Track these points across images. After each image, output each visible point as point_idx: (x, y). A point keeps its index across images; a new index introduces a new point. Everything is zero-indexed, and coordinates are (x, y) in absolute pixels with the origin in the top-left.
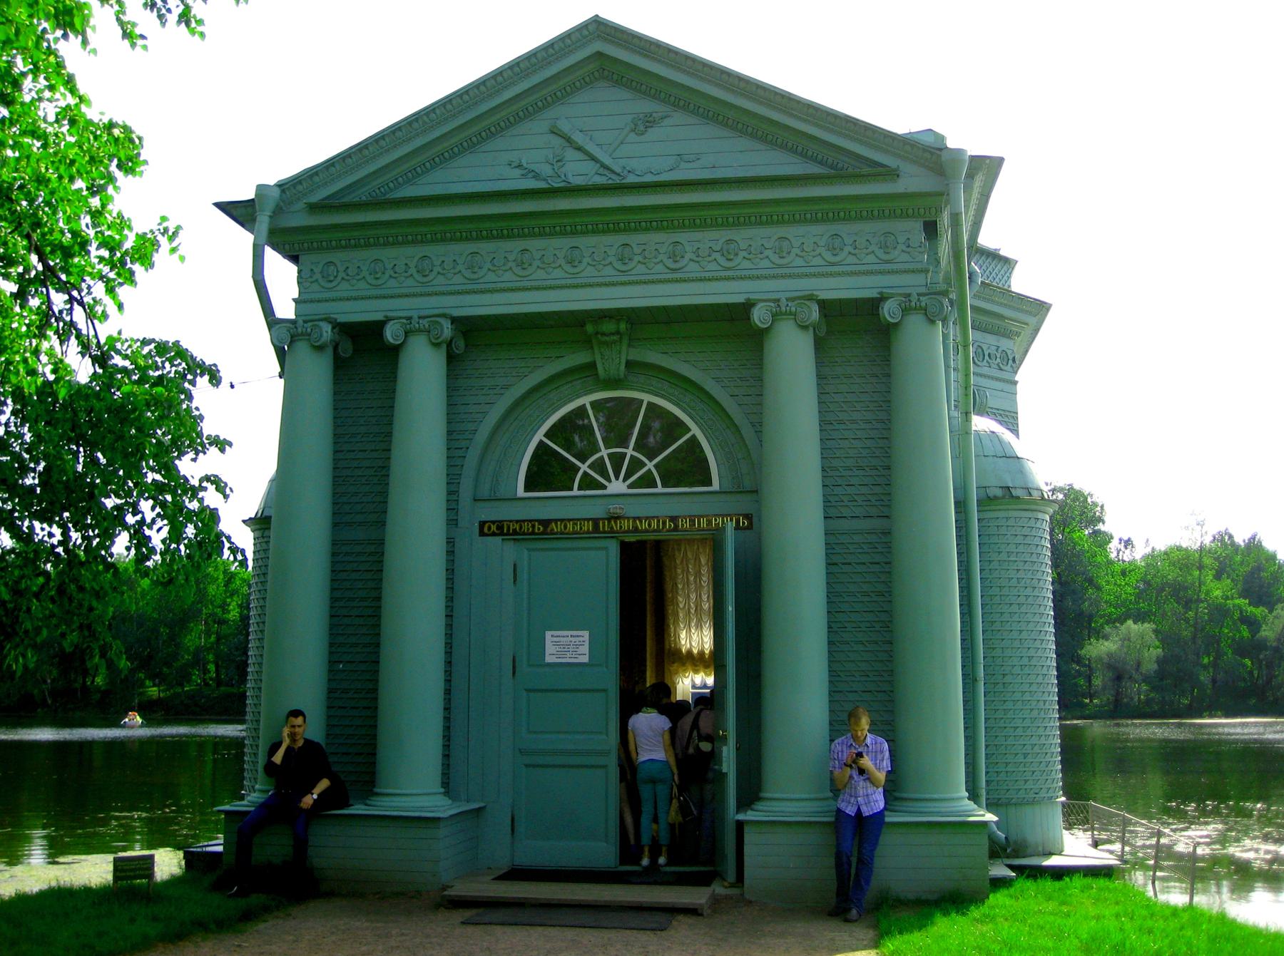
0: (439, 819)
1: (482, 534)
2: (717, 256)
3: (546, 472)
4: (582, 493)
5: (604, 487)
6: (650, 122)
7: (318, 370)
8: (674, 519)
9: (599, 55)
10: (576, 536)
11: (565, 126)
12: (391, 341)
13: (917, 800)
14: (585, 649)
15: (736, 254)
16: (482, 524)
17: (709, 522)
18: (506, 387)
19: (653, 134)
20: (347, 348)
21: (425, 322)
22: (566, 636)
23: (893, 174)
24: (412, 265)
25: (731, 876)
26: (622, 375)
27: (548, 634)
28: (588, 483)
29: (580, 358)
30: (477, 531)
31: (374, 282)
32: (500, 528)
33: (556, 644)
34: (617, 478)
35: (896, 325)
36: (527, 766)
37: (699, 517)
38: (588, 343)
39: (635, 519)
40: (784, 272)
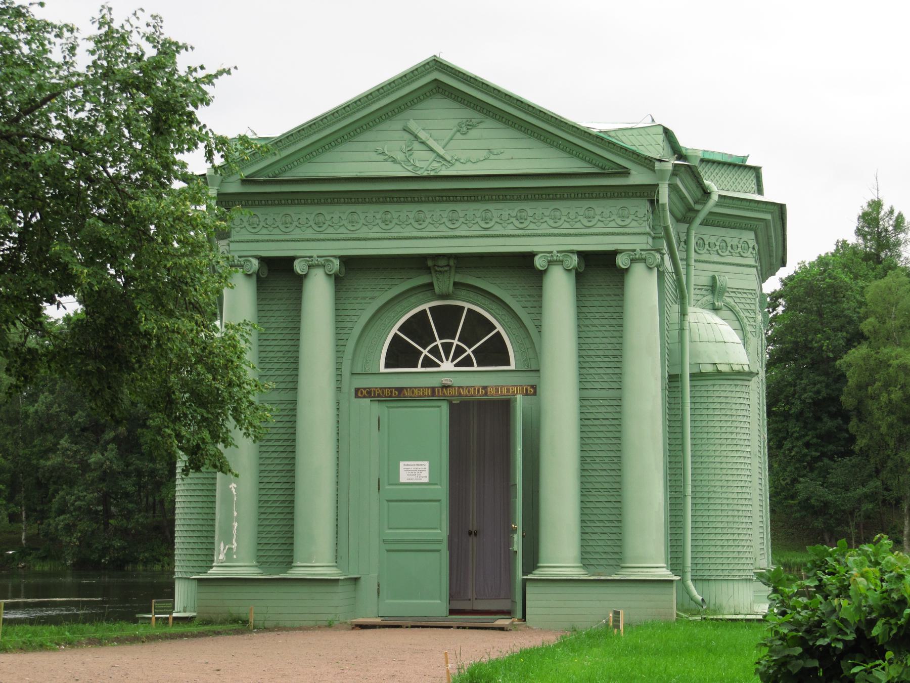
0: (338, 580)
1: (357, 396)
2: (513, 220)
3: (400, 355)
4: (424, 369)
5: (439, 366)
6: (470, 127)
8: (485, 388)
9: (436, 80)
12: (300, 272)
13: (623, 567)
14: (426, 473)
16: (357, 390)
17: (508, 390)
19: (473, 133)
22: (413, 465)
23: (626, 173)
25: (519, 614)
27: (402, 464)
28: (428, 363)
29: (423, 280)
31: (285, 230)
33: (407, 470)
34: (447, 360)
35: (627, 270)
36: (388, 551)
37: (502, 387)
38: (428, 270)
39: (459, 387)
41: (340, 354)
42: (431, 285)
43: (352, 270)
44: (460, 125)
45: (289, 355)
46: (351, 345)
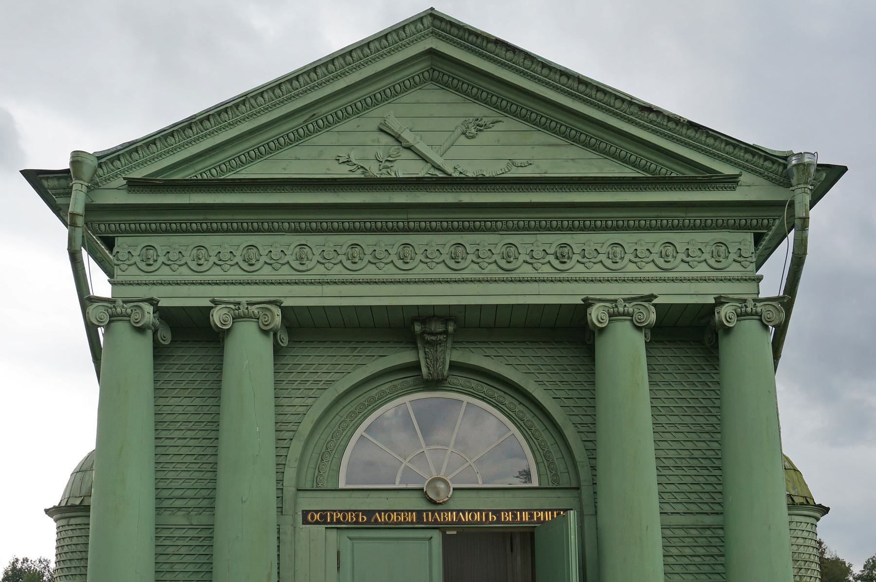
1: (305, 522)
6: (481, 128)
7: (138, 352)
8: (497, 512)
9: (432, 53)
10: (397, 526)
11: (395, 125)
15: (622, 258)
16: (305, 513)
17: (531, 516)
18: (330, 382)
19: (483, 137)
20: (165, 336)
21: (254, 309)
24: (238, 253)
26: (445, 373)
29: (405, 357)
30: (300, 519)
32: (323, 517)
35: (602, 330)
37: (521, 511)
38: (411, 341)
39: (458, 511)
40: (623, 275)
41: (281, 460)
42: (415, 367)
43: (303, 330)
44: (466, 124)
45: (205, 459)
46: (296, 448)
